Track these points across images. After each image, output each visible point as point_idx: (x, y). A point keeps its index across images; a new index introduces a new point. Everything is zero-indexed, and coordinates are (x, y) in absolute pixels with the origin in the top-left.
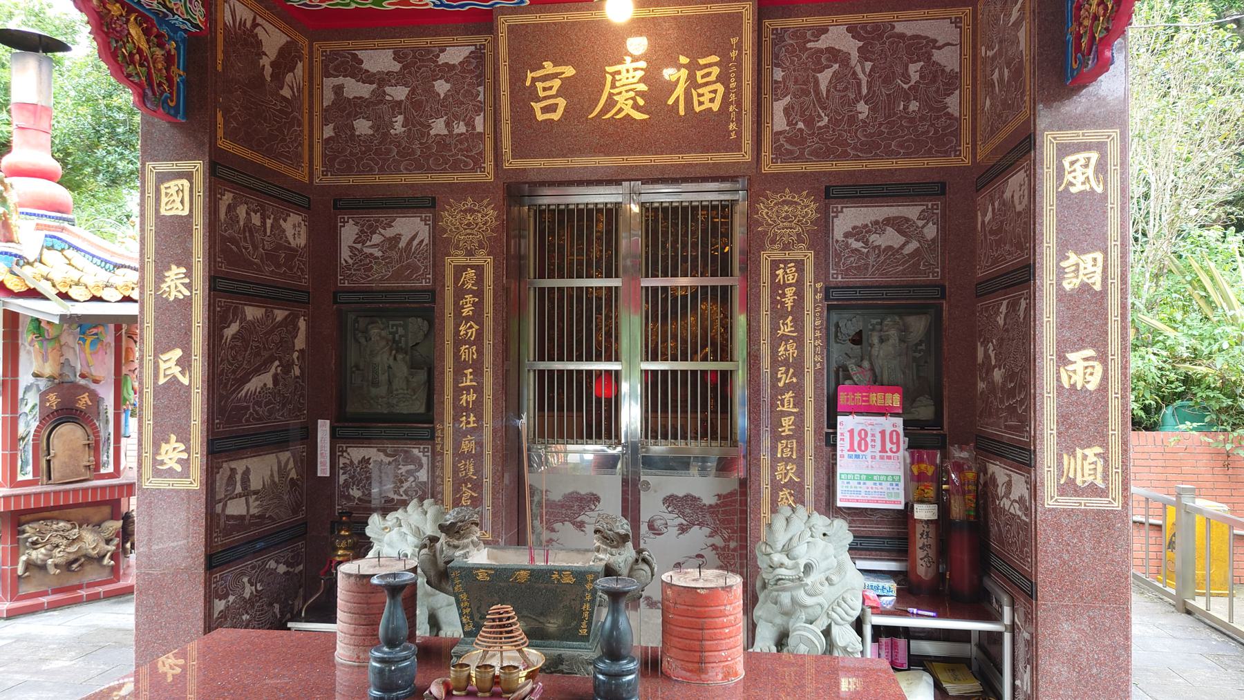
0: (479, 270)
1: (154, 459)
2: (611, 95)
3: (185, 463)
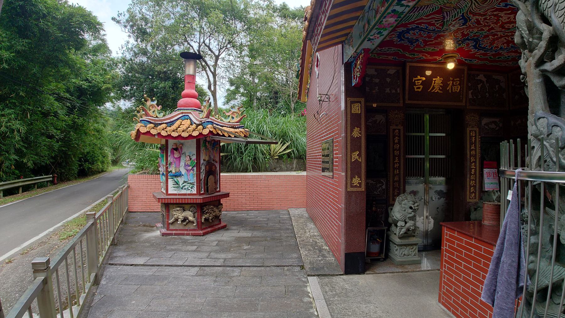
0: (399, 130)
1: (351, 182)
2: (434, 86)
3: (360, 184)
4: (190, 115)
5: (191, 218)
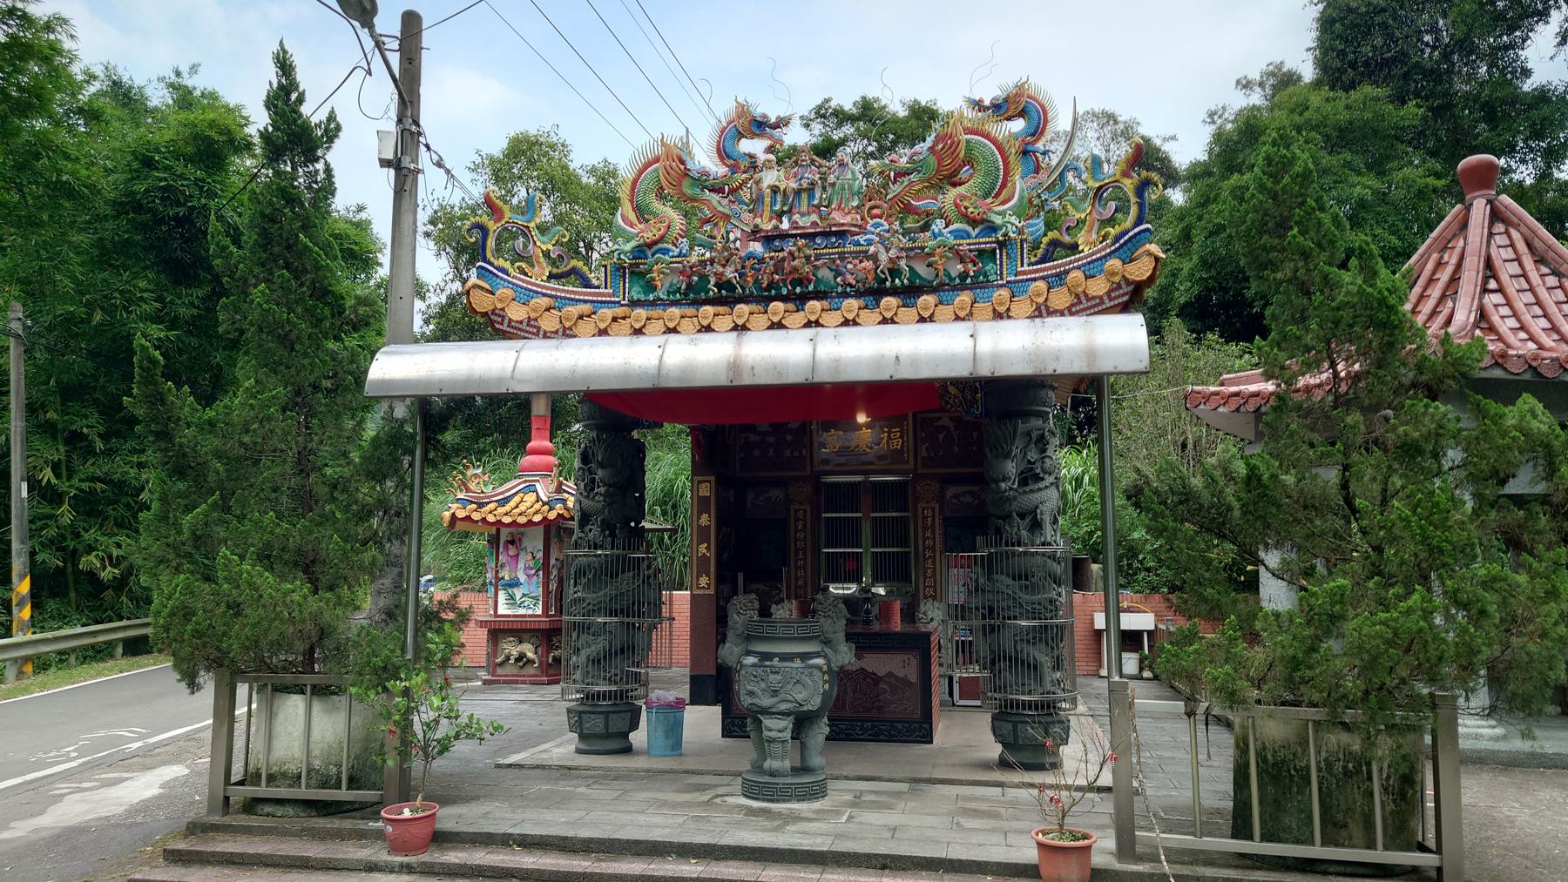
4: (538, 485)
5: (530, 655)
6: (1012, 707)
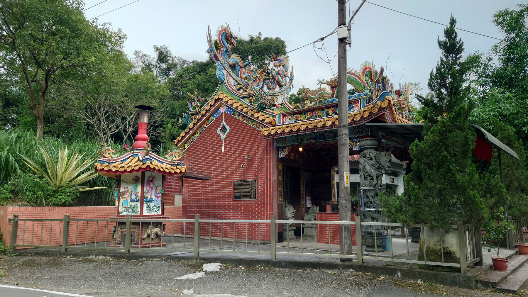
6: (367, 234)
